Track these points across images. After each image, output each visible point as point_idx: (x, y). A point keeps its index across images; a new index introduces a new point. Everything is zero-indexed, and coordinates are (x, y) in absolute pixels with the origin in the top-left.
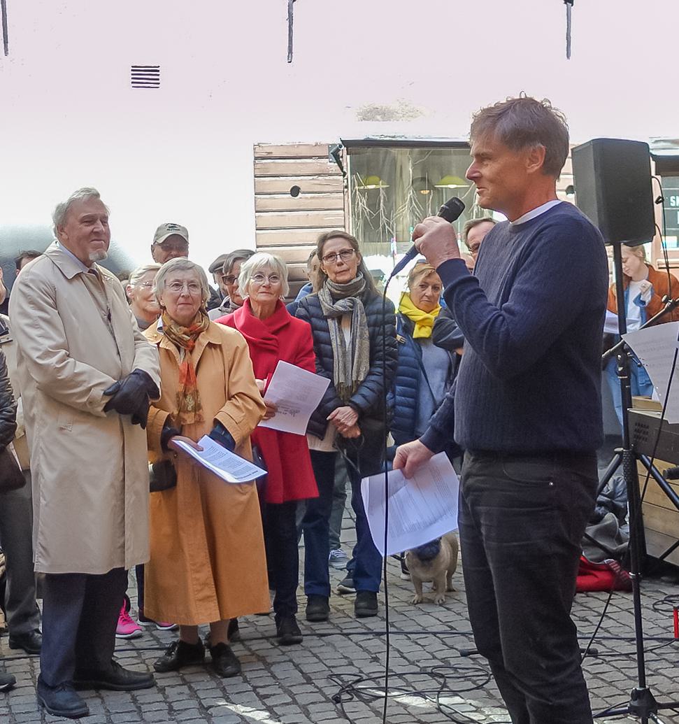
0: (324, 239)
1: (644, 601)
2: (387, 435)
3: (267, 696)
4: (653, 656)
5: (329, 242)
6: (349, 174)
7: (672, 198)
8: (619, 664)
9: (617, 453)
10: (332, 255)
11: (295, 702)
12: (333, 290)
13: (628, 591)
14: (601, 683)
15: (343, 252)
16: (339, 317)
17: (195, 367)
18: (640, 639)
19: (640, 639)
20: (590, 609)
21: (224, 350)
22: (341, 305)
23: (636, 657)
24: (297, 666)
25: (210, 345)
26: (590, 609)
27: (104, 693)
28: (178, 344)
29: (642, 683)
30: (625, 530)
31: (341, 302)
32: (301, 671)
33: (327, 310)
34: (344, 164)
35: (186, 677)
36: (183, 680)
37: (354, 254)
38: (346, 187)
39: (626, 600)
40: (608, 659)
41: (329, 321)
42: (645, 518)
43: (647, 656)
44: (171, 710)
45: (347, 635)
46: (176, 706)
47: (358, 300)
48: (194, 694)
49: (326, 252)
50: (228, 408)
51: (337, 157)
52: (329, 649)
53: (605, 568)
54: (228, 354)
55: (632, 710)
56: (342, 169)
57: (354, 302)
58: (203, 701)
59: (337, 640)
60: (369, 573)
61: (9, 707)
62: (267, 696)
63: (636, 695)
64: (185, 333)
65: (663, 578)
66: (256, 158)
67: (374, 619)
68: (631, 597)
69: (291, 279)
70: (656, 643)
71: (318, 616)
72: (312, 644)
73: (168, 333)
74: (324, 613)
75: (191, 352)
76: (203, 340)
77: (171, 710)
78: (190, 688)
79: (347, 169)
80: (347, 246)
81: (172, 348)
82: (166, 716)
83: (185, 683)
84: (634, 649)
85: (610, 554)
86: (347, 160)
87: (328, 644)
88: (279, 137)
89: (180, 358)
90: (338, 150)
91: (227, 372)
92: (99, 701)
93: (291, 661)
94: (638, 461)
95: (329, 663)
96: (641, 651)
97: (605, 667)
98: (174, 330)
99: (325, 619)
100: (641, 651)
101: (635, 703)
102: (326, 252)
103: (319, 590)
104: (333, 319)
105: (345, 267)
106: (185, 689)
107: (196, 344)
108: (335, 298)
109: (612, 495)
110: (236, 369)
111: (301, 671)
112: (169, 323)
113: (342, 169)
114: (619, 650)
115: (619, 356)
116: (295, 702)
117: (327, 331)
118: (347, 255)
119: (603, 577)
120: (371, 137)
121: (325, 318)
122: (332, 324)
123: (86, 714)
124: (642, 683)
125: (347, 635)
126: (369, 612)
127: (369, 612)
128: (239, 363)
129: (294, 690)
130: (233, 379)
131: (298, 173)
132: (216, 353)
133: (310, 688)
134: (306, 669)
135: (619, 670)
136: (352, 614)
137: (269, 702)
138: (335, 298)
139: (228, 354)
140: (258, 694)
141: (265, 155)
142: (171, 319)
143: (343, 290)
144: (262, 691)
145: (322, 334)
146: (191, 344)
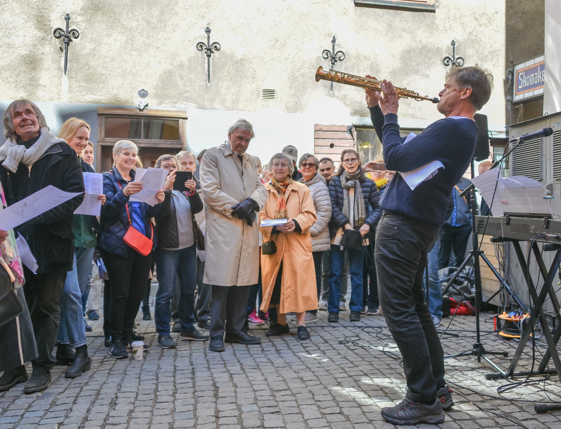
0: (344, 152)
1: (480, 319)
2: (367, 275)
3: (307, 347)
4: (484, 338)
5: (346, 154)
6: (356, 140)
7: (498, 156)
8: (468, 340)
9: (470, 252)
10: (347, 160)
11: (319, 349)
12: (347, 176)
13: (474, 315)
14: (459, 347)
15: (353, 159)
16: (348, 189)
17: (286, 200)
18: (478, 331)
19: (478, 331)
20: (456, 321)
21: (299, 193)
22: (350, 183)
23: (476, 338)
24: (321, 337)
25: (293, 191)
26: (456, 321)
27: (233, 344)
28: (279, 190)
29: (478, 340)
30: (473, 290)
31: (350, 182)
32: (323, 339)
33: (344, 185)
34: (354, 135)
35: (271, 339)
36: (270, 340)
37: (357, 160)
38: (354, 145)
39: (474, 319)
40: (463, 338)
41: (344, 190)
42: (483, 285)
43: (481, 338)
44: (263, 350)
45: (345, 327)
46: (265, 349)
47: (358, 182)
48: (274, 345)
49: (345, 158)
50: (301, 216)
51: (350, 132)
52: (337, 332)
53: (463, 305)
54: (301, 195)
55: (474, 353)
56: (353, 137)
57: (356, 183)
58: (278, 348)
59: (341, 329)
60: (355, 303)
61: (190, 347)
62: (307, 347)
63: (475, 346)
64: (281, 185)
65: (490, 312)
66: (315, 131)
67: (359, 322)
68: (475, 318)
69: (339, 90)
70: (485, 333)
71: (333, 320)
72: (330, 330)
73: (274, 186)
74: (336, 319)
75: (284, 194)
76: (290, 188)
77: (263, 350)
78: (273, 343)
79: (355, 137)
80: (355, 157)
81: (276, 192)
82: (260, 352)
83: (270, 341)
84: (475, 335)
85: (467, 299)
86: (355, 133)
87: (337, 330)
88: (325, 122)
89: (279, 196)
90: (351, 129)
91: (301, 203)
92: (230, 346)
93: (319, 335)
94: (480, 257)
95: (336, 336)
96: (478, 336)
97: (462, 341)
98: (277, 184)
99: (337, 322)
100: (478, 336)
101: (475, 350)
102: (345, 158)
103: (335, 310)
104: (346, 189)
105: (352, 166)
106: (270, 343)
107: (286, 190)
108: (347, 180)
109: (468, 274)
110: (305, 200)
111: (323, 339)
112: (275, 181)
113: (353, 137)
114: (468, 335)
115: (471, 210)
116: (319, 349)
117: (342, 193)
118: (354, 161)
119: (463, 308)
120: (366, 124)
121: (343, 188)
122: (345, 191)
123: (223, 351)
124: (478, 340)
125: (345, 327)
126: (356, 319)
127: (356, 319)
128: (306, 199)
129: (319, 345)
130: (303, 206)
131: (333, 138)
132: (295, 195)
133: (327, 345)
134: (325, 338)
135: (468, 342)
136: (349, 321)
137: (307, 349)
138: (347, 180)
139: (301, 195)
140: (303, 346)
141: (319, 129)
142: (275, 179)
143: (352, 176)
144: (304, 345)
145: (340, 194)
146: (284, 190)
